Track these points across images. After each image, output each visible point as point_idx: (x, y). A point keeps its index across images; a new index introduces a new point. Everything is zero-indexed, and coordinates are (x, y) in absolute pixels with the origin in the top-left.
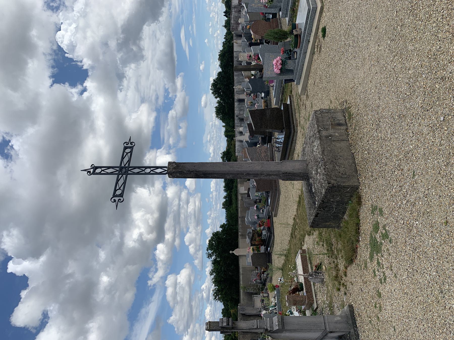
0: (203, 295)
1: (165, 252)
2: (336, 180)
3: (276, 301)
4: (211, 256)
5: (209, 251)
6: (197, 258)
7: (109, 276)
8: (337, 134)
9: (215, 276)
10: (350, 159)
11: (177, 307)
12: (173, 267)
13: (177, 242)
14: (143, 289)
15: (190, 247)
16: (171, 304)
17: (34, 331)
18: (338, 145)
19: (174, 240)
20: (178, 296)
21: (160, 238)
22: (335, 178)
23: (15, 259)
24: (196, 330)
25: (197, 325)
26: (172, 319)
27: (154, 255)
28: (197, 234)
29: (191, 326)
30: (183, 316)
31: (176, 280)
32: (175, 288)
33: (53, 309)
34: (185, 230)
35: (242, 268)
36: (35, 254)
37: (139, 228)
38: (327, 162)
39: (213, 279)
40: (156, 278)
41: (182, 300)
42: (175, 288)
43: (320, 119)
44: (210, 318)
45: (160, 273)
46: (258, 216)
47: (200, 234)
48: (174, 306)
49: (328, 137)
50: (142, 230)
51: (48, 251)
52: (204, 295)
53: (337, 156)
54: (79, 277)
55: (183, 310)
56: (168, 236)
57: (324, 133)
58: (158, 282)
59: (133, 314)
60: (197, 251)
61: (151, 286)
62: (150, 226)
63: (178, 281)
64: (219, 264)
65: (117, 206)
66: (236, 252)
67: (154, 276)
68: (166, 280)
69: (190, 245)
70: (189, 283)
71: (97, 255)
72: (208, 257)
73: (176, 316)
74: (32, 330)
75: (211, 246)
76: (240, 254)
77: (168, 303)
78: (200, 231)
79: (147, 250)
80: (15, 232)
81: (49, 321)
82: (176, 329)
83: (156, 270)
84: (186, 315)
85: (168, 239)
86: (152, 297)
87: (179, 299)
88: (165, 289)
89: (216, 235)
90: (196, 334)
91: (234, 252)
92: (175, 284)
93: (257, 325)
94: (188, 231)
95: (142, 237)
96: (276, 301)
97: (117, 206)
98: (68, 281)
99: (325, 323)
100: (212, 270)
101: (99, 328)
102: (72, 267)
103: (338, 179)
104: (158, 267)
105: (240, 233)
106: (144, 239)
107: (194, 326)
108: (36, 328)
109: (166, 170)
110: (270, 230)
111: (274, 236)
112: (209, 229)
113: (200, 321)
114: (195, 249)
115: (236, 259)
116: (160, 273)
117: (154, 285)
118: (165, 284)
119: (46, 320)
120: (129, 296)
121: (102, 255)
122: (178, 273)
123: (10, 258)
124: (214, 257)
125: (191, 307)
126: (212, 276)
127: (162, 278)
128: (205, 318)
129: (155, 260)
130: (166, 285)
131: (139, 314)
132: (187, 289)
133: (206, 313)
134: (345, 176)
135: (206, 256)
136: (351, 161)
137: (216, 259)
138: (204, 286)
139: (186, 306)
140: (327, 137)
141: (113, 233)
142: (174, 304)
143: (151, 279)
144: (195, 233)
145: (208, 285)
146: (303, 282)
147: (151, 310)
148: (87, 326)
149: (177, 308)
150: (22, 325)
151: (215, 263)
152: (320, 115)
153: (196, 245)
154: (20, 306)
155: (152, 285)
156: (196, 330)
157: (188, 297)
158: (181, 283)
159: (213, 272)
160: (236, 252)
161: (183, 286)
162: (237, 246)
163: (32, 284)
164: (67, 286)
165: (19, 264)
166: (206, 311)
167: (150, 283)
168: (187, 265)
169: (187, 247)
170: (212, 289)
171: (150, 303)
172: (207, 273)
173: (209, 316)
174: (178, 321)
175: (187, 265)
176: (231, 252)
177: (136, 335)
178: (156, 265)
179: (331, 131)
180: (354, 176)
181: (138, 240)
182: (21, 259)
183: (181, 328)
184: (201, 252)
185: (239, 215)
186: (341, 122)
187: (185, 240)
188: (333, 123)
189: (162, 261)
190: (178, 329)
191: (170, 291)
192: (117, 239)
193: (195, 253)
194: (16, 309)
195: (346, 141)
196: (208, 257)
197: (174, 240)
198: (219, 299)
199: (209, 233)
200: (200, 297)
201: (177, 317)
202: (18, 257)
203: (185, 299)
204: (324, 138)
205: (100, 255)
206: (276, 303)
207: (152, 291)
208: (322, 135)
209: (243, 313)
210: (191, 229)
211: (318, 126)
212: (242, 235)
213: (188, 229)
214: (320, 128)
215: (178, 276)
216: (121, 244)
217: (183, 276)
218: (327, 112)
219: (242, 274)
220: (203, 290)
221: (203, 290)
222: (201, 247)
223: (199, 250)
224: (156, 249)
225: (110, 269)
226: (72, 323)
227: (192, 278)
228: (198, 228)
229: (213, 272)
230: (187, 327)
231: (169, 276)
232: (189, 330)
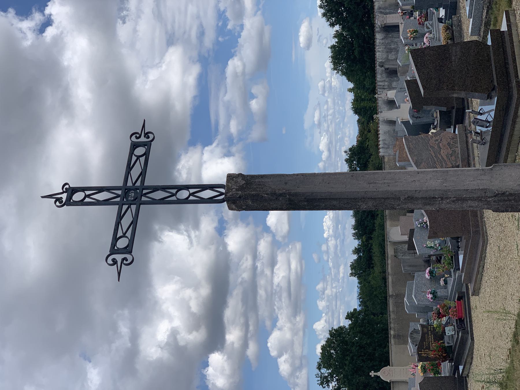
4: (328, 382)
5: (324, 370)
13: (252, 350)
19: (245, 345)
21: (215, 340)
27: (204, 377)
28: (295, 332)
34: (268, 323)
37: (171, 319)
46: (434, 293)
47: (301, 333)
50: (177, 323)
56: (233, 336)
60: (296, 369)
62: (193, 314)
69: (280, 355)
76: (394, 379)
78: (301, 325)
85: (233, 343)
89: (337, 336)
91: (378, 374)
95: (175, 339)
105: (392, 332)
106: (182, 343)
110: (464, 324)
111: (473, 339)
114: (292, 365)
124: (334, 384)
135: (316, 381)
141: (114, 328)
153: (293, 357)
162: (386, 362)
176: (372, 374)
181: (167, 344)
184: (304, 372)
185: (391, 290)
187: (269, 345)
192: (123, 342)
193: (292, 374)
197: (245, 345)
205: (89, 376)
210: (282, 320)
213: (274, 321)
216: (132, 354)
222: (304, 362)
223: (301, 368)
224: (206, 365)
228: (298, 319)
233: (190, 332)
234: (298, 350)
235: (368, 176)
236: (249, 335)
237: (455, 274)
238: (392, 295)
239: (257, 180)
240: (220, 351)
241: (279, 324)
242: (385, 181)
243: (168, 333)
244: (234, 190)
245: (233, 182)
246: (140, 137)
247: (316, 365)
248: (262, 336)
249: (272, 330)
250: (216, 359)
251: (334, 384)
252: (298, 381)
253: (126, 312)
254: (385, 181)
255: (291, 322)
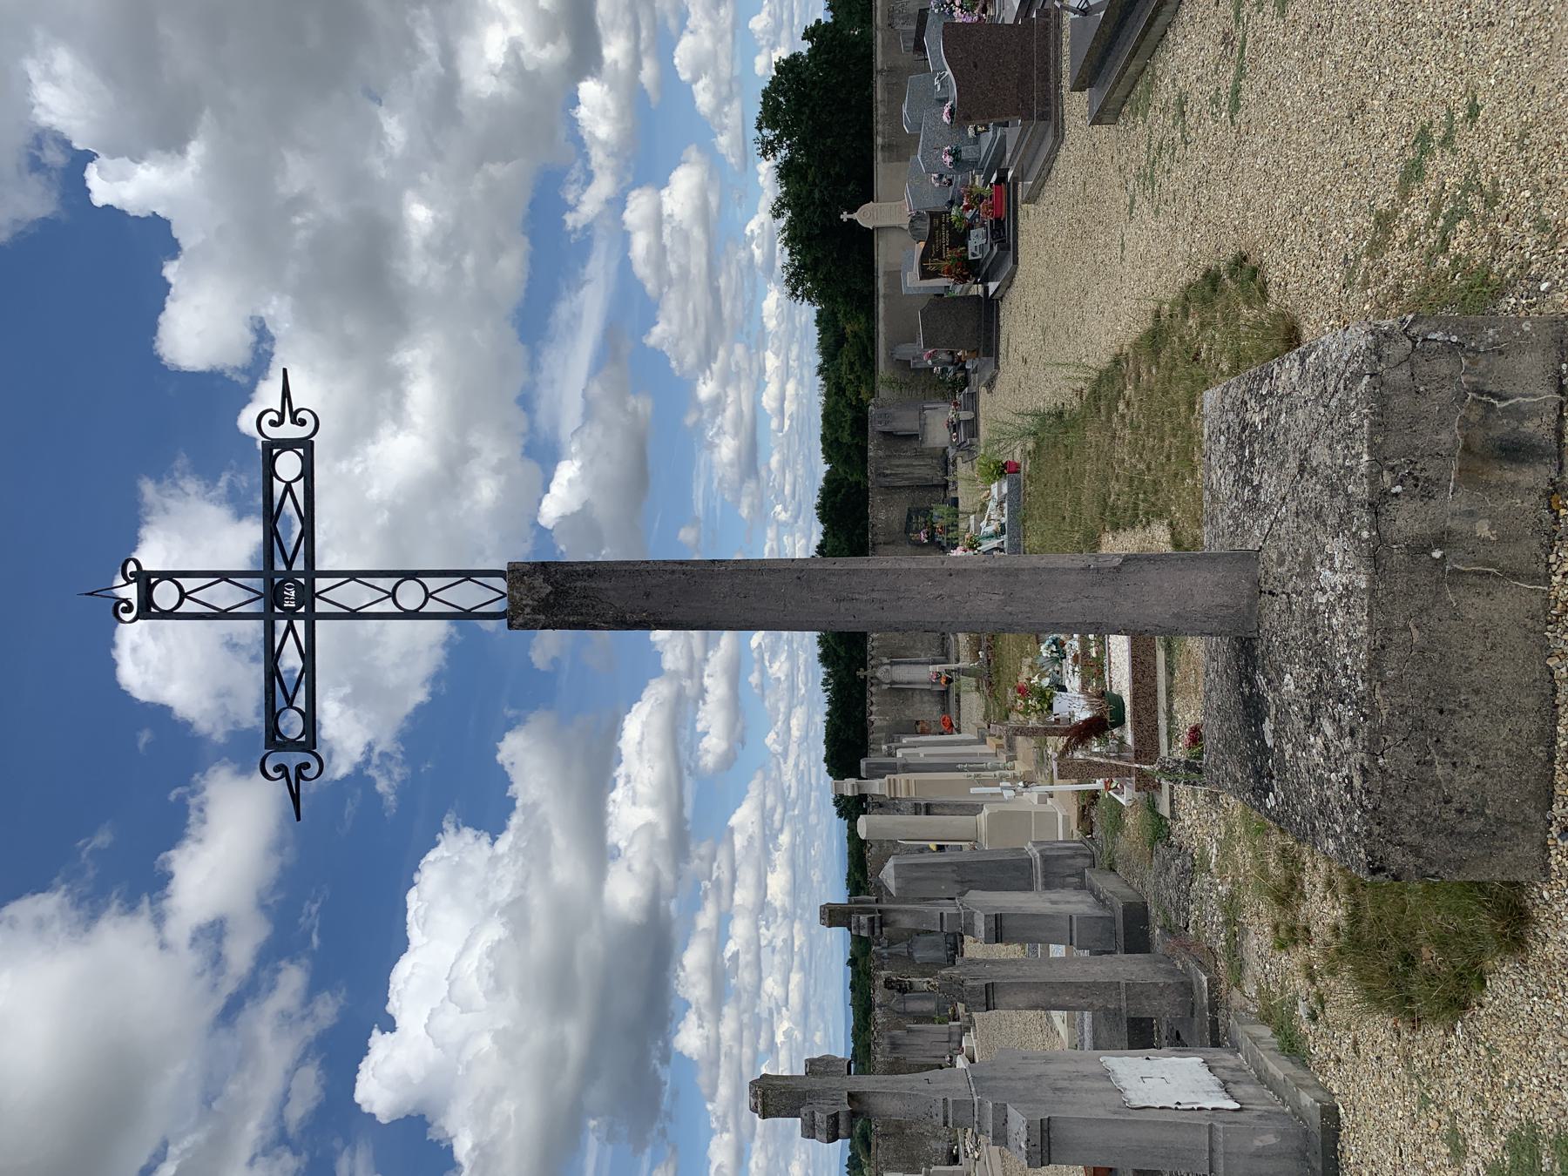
0: (752, 255)
1: (613, 113)
2: (1416, 851)
3: (1004, 520)
4: (773, 150)
5: (766, 132)
6: (723, 128)
7: (430, 203)
8: (1483, 529)
9: (789, 221)
10: (1524, 713)
11: (672, 295)
12: (645, 163)
13: (648, 73)
14: (549, 244)
15: (698, 87)
16: (650, 287)
17: (244, 380)
18: (1475, 606)
19: (636, 65)
20: (669, 259)
21: (585, 59)
22: (1416, 838)
23: (103, 159)
24: (737, 364)
25: (739, 349)
27: (574, 123)
28: (718, 37)
29: (721, 353)
30: (691, 321)
31: (659, 207)
32: (659, 234)
33: (278, 311)
34: (672, 23)
35: (885, 273)
36: (167, 138)
37: (506, 24)
38: (1389, 729)
39: (783, 230)
40: (590, 203)
41: (685, 273)
42: (659, 234)
43: (1400, 402)
44: (779, 325)
45: (603, 187)
46: (955, 154)
47: (729, 38)
48: (661, 294)
49: (1427, 550)
50: (518, 30)
51: (206, 118)
52: (757, 253)
53: (1455, 689)
54: (332, 209)
55: (691, 305)
56: (614, 50)
57: (1407, 520)
58: (600, 215)
59: (533, 321)
60: (722, 100)
61: (575, 230)
62: (544, 13)
63: (666, 210)
64: (804, 177)
66: (865, 216)
67: (584, 198)
68: (624, 208)
69: (696, 80)
70: (703, 213)
71: (372, 131)
72: (764, 154)
73: (670, 321)
74: (235, 377)
75: (770, 115)
76: (879, 224)
77: (640, 285)
78: (727, 23)
79: (544, 106)
80: (64, 60)
81: (276, 349)
82: (674, 364)
83: (589, 178)
84: (702, 318)
85: (616, 62)
86: (584, 267)
87: (673, 268)
88: (625, 238)
89: (788, 68)
90: (738, 373)
91: (855, 216)
92: (658, 220)
93: (946, 1117)
94: (682, 26)
95: (518, 57)
96: (1004, 520)
98: (298, 220)
99: (1212, 1151)
100: (779, 200)
102: (297, 173)
103: (1431, 845)
104: (593, 165)
105: (879, 140)
106: (530, 67)
107: (730, 352)
108: (245, 371)
110: (1004, 233)
111: (1016, 262)
112: (764, 14)
113: (748, 335)
114: (716, 94)
115: (865, 239)
116: (603, 187)
117: (587, 227)
118: (623, 223)
119: (266, 346)
120: (511, 267)
121: (395, 130)
122: (664, 183)
123: (89, 157)
124: (784, 152)
125: (714, 291)
126: (782, 222)
127: (608, 202)
128: (763, 327)
129: (578, 143)
130: (628, 227)
132: (697, 233)
133: (765, 313)
134: (1477, 825)
135: (756, 149)
136: (1530, 725)
137: (792, 159)
138: (752, 226)
139: (699, 292)
140: (1419, 548)
141: (410, 40)
142: (660, 288)
143: (573, 209)
144: (712, 32)
145: (762, 230)
146: (1127, 700)
147: (588, 307)
148: (394, 358)
149: (671, 302)
150: (201, 366)
151: (787, 172)
152: (1402, 374)
153: (717, 81)
154: (172, 308)
155: (580, 226)
156: (737, 364)
157: (704, 261)
158: (677, 218)
159: (783, 205)
160: (865, 216)
161: (684, 226)
162: (867, 195)
163: (188, 235)
164: (302, 234)
165: (123, 177)
166: (765, 304)
167: (570, 219)
168: (692, 153)
169: (686, 91)
170: (779, 264)
171: (580, 286)
172: (761, 179)
175: (692, 153)
176: (845, 216)
177: (552, 382)
178: (586, 158)
179: (1452, 503)
180: (1526, 825)
181: (505, 67)
182: (126, 159)
183: (690, 359)
184: (736, 104)
185: (879, 61)
186: (1529, 427)
187: (676, 61)
188: (1479, 435)
189: (604, 144)
190: (680, 363)
191: (640, 244)
192: (430, 66)
193: (718, 109)
194: (162, 318)
195: (1534, 578)
196: (764, 154)
197: (636, 65)
198: (807, 295)
199: (764, 67)
200: (744, 263)
201: (675, 328)
202: (114, 154)
203: (694, 271)
204: (1398, 556)
205: (386, 128)
206: (1002, 525)
207: (583, 246)
208: (1391, 532)
209: (887, 429)
210: (697, 17)
211: (1379, 460)
212: (887, 147)
213: (683, 16)
214: (1387, 477)
215: (665, 192)
216: (449, 85)
217: (682, 191)
218: (1452, 348)
219: (885, 296)
220: (752, 238)
221: (752, 238)
222: (735, 88)
223: (728, 99)
224: (575, 101)
225: (430, 176)
226: (347, 350)
227: (713, 200)
228: (722, 12)
229: (783, 205)
230: (707, 357)
231: (634, 194)
232: (715, 367)
233: (542, 46)
234: (725, 71)
235: (834, 579)
236: (642, 46)
237: (995, 133)
238: (882, 70)
239: (578, 584)
240: (592, 75)
241: (690, 23)
242: (875, 595)
243: (505, 49)
244: (528, 610)
245: (523, 588)
246: (282, 421)
247: (755, 122)
248: (664, 46)
249: (681, 33)
250: (590, 91)
251: (784, 152)
252: (726, 121)
253: (426, 12)
254: (875, 595)
255: (711, 18)
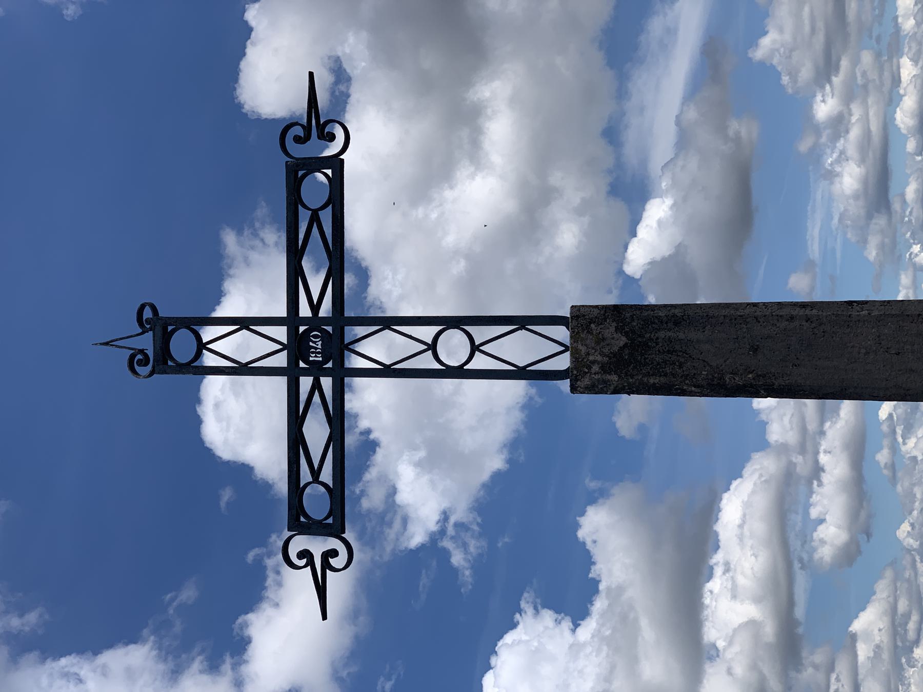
25: (867, 58)
26: (768, 44)
29: (845, 63)
30: (807, 28)
33: (355, 48)
65: (107, 344)
73: (781, 30)
82: (785, 79)
84: (820, 25)
90: (865, 87)
97: (107, 344)
101: (513, 101)
107: (856, 61)
109: (317, 386)
113: (878, 39)
119: (342, 88)
131: (642, 38)
133: (900, 12)
156: (864, 74)
173: (912, 22)
174: (791, 51)
177: (642, 110)
183: (806, 73)
190: (793, 76)
194: (243, 64)
201: (787, 37)
226: (424, 86)
232: (836, 80)
